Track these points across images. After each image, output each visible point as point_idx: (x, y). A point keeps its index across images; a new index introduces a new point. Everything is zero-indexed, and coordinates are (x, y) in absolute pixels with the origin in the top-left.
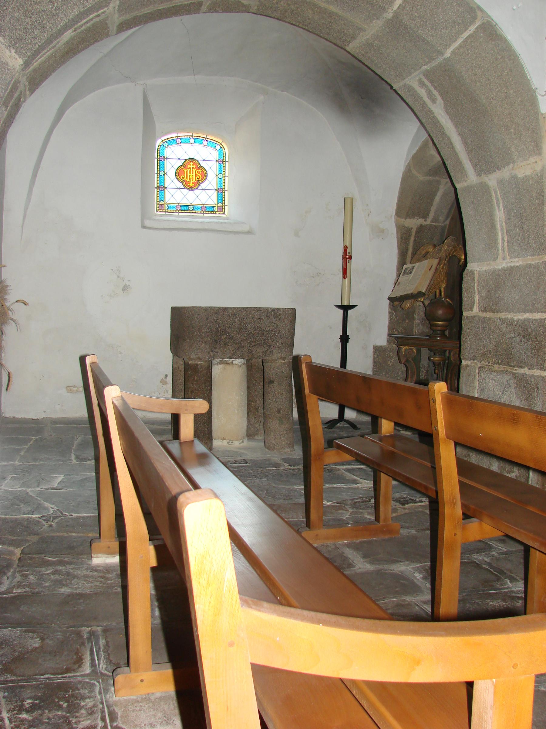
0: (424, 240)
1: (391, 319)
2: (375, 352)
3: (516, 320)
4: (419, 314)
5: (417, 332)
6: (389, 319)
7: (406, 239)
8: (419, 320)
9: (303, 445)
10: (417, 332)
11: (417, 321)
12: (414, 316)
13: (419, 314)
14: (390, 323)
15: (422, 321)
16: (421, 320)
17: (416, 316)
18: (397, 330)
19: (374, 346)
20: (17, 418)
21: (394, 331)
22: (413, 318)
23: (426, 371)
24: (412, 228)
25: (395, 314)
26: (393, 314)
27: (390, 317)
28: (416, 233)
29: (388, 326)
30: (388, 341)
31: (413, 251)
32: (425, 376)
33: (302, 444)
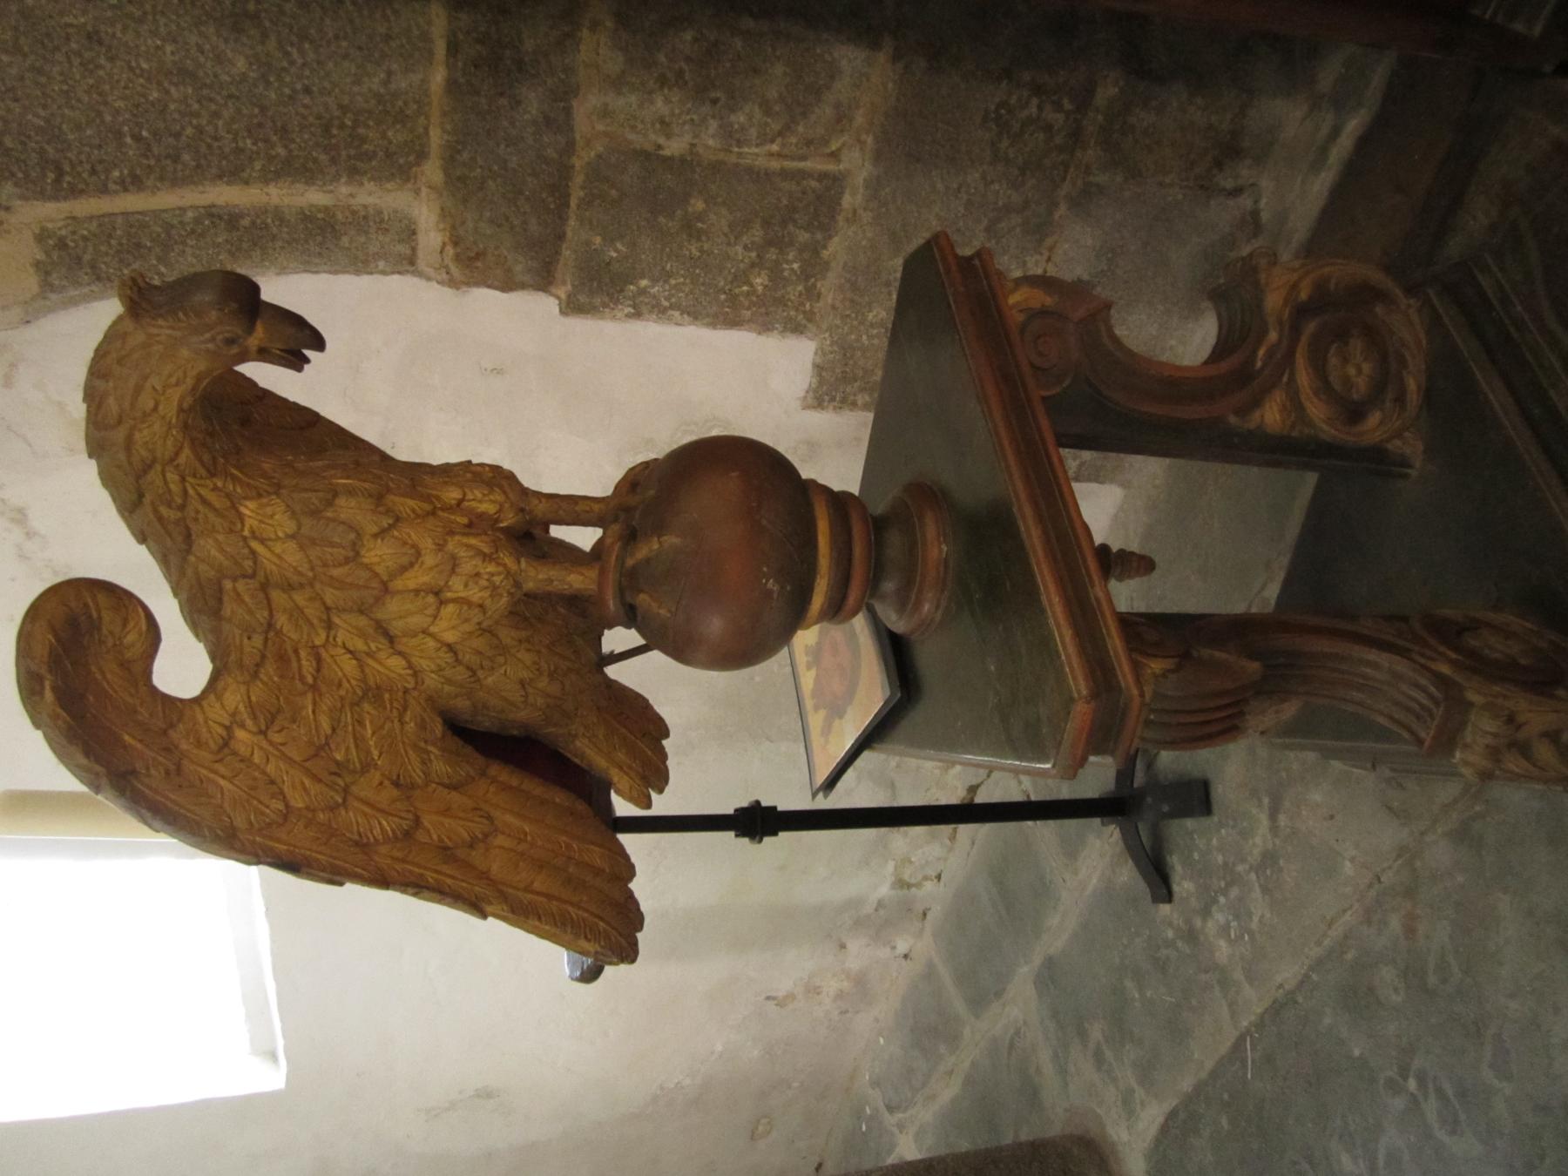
0: (117, 112)
1: (672, 307)
2: (843, 401)
3: (388, 496)
4: (664, 124)
5: (775, 148)
6: (670, 319)
7: (138, 245)
8: (704, 120)
9: (962, 1159)
10: (775, 148)
11: (710, 140)
12: (671, 158)
13: (664, 124)
14: (695, 314)
15: (715, 102)
16: (706, 109)
17: (675, 147)
18: (741, 278)
19: (806, 407)
20: (1131, 354)
21: (748, 294)
22: (683, 165)
23: (1035, 101)
24: (41, 237)
25: (644, 283)
26: (643, 292)
27: (660, 311)
28: (75, 192)
29: (713, 325)
30: (797, 329)
31: (220, 177)
32: (1058, 107)
33: (964, 1146)
